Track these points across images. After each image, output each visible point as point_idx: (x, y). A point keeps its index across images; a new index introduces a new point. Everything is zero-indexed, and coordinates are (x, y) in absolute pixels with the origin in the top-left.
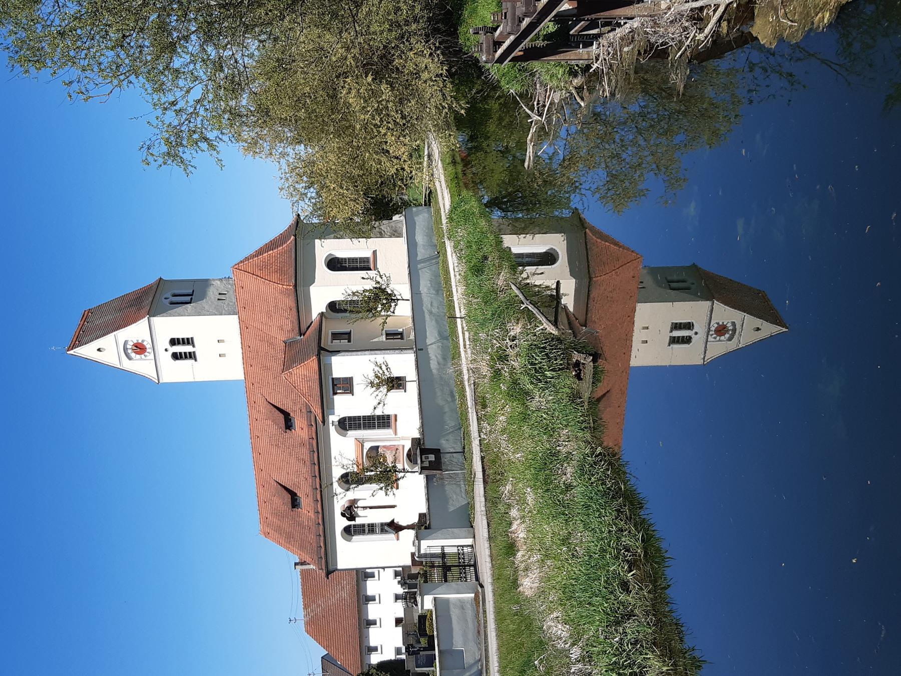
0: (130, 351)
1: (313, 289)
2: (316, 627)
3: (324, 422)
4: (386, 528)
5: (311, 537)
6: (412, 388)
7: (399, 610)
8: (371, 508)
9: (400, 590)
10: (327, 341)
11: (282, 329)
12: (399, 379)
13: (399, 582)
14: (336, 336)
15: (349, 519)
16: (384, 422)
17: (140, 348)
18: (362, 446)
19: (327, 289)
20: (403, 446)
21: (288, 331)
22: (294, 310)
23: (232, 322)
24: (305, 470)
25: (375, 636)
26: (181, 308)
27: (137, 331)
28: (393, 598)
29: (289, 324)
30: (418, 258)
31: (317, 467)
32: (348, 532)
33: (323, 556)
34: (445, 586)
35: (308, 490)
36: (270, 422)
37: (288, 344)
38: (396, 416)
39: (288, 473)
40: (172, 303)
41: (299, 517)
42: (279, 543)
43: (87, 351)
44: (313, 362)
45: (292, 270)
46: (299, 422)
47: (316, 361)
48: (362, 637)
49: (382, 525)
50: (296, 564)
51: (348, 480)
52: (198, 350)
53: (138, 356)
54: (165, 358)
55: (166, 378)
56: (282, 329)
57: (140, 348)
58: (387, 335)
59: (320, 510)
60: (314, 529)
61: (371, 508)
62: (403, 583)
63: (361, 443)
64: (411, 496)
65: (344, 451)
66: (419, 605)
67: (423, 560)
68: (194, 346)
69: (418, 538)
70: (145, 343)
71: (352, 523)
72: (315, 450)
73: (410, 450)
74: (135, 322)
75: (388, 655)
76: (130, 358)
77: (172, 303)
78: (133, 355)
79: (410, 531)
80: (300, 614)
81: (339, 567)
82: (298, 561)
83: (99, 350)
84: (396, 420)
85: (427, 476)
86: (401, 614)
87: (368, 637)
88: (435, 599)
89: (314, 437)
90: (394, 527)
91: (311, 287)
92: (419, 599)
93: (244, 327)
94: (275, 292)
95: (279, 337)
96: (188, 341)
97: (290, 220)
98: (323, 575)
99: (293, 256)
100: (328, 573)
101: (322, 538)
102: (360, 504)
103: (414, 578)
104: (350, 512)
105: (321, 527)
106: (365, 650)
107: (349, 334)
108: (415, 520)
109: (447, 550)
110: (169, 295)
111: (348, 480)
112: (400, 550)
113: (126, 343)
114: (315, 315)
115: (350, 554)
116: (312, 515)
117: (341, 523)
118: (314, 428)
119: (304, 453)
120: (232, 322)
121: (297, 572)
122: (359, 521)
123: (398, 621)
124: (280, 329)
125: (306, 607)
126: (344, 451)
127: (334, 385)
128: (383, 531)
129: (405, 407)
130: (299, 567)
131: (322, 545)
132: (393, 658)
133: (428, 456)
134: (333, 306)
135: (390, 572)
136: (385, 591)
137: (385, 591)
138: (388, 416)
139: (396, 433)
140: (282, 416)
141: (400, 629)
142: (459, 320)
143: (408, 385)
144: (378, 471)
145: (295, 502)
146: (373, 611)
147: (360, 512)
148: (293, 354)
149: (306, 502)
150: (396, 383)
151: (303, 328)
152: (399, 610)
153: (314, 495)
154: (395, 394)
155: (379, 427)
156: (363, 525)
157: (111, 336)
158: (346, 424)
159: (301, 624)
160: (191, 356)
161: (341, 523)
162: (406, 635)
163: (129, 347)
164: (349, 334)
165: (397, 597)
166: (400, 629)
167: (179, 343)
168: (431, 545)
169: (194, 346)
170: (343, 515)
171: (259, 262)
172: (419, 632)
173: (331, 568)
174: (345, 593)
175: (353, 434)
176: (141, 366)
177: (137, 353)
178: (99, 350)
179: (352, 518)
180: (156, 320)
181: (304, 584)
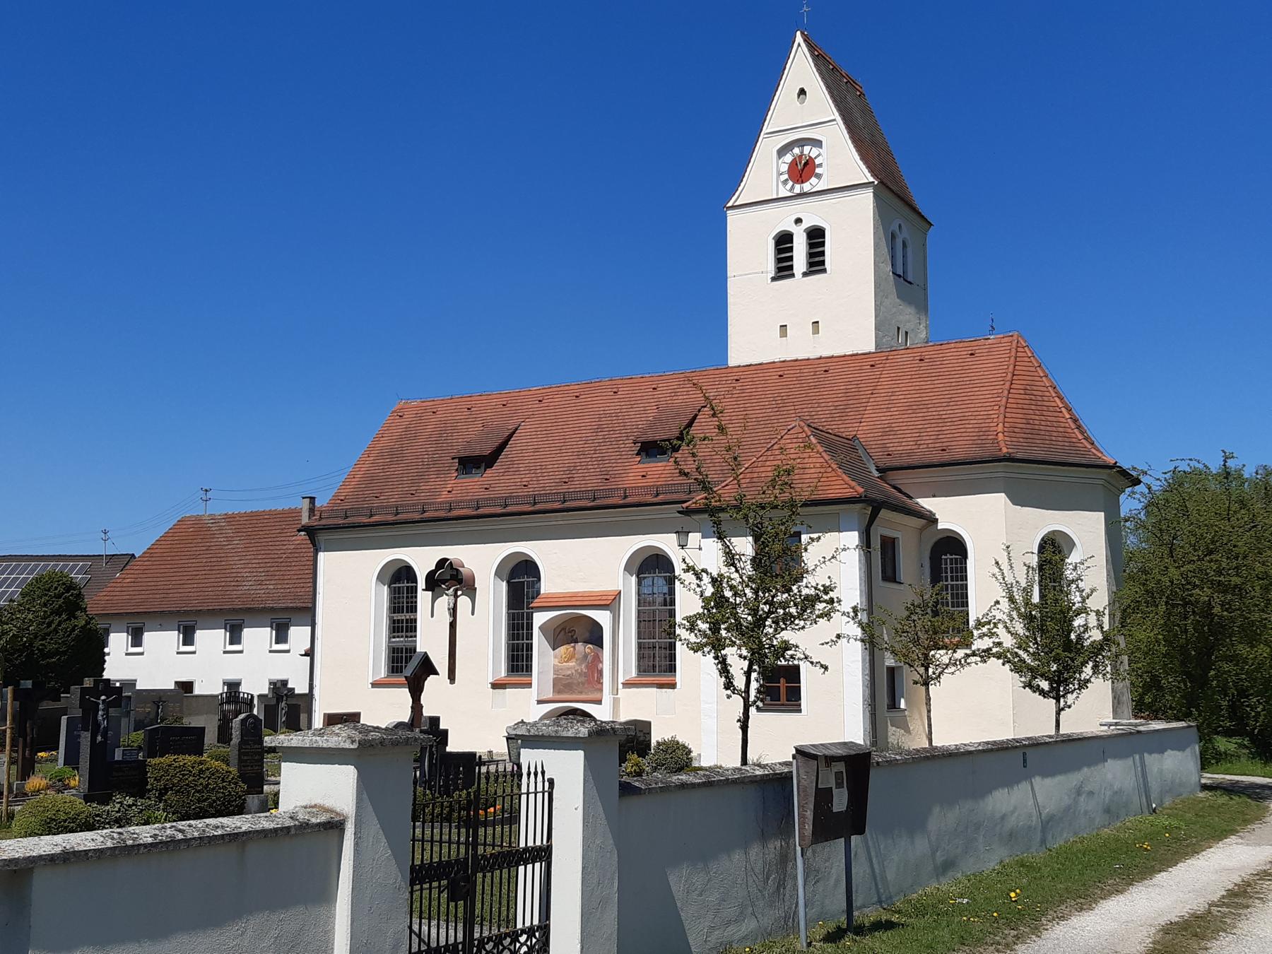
0: (797, 151)
1: (998, 501)
2: (190, 538)
5: (392, 497)
8: (453, 626)
10: (890, 523)
11: (885, 433)
14: (889, 546)
15: (430, 577)
17: (802, 170)
19: (993, 532)
20: (599, 702)
21: (884, 446)
22: (946, 457)
23: (864, 341)
24: (547, 483)
25: (161, 642)
26: (885, 250)
27: (841, 159)
28: (232, 677)
29: (903, 446)
30: (1146, 755)
31: (557, 505)
32: (400, 578)
33: (350, 520)
34: (394, 877)
35: (501, 490)
36: (652, 413)
38: (673, 686)
39: (536, 450)
40: (893, 236)
41: (438, 473)
42: (378, 439)
43: (801, 67)
44: (841, 486)
45: (1040, 455)
47: (848, 493)
48: (161, 619)
50: (312, 499)
51: (521, 579)
52: (799, 282)
53: (785, 168)
55: (735, 222)
56: (885, 433)
57: (802, 170)
58: (891, 671)
59: (455, 513)
60: (411, 500)
61: (453, 626)
63: (611, 603)
68: (805, 274)
70: (813, 180)
71: (421, 584)
72: (598, 502)
74: (864, 158)
76: (782, 152)
77: (893, 236)
78: (788, 158)
80: (220, 507)
81: (321, 555)
82: (318, 504)
83: (802, 92)
84: (661, 686)
85: (787, 778)
87: (162, 628)
88: (334, 826)
89: (629, 500)
91: (1002, 496)
94: (983, 417)
95: (864, 427)
96: (816, 263)
99: (1071, 460)
101: (391, 518)
102: (464, 601)
104: (449, 578)
106: (137, 622)
111: (521, 579)
113: (817, 143)
114: (927, 503)
115: (349, 582)
116: (444, 497)
117: (422, 559)
118: (650, 499)
119: (587, 481)
120: (864, 341)
122: (424, 597)
123: (186, 686)
124: (884, 428)
125: (230, 518)
126: (585, 566)
130: (305, 504)
134: (950, 551)
136: (248, 663)
137: (248, 663)
138: (672, 669)
139: (627, 685)
145: (470, 463)
146: (211, 639)
147: (444, 602)
149: (474, 485)
151: (901, 479)
153: (491, 501)
155: (640, 647)
156: (413, 609)
160: (784, 269)
161: (422, 559)
162: (157, 697)
163: (807, 149)
167: (811, 246)
169: (805, 274)
170: (442, 563)
171: (1030, 393)
173: (322, 538)
174: (251, 588)
175: (628, 587)
176: (764, 171)
177: (793, 165)
178: (802, 92)
179: (433, 583)
180: (867, 197)
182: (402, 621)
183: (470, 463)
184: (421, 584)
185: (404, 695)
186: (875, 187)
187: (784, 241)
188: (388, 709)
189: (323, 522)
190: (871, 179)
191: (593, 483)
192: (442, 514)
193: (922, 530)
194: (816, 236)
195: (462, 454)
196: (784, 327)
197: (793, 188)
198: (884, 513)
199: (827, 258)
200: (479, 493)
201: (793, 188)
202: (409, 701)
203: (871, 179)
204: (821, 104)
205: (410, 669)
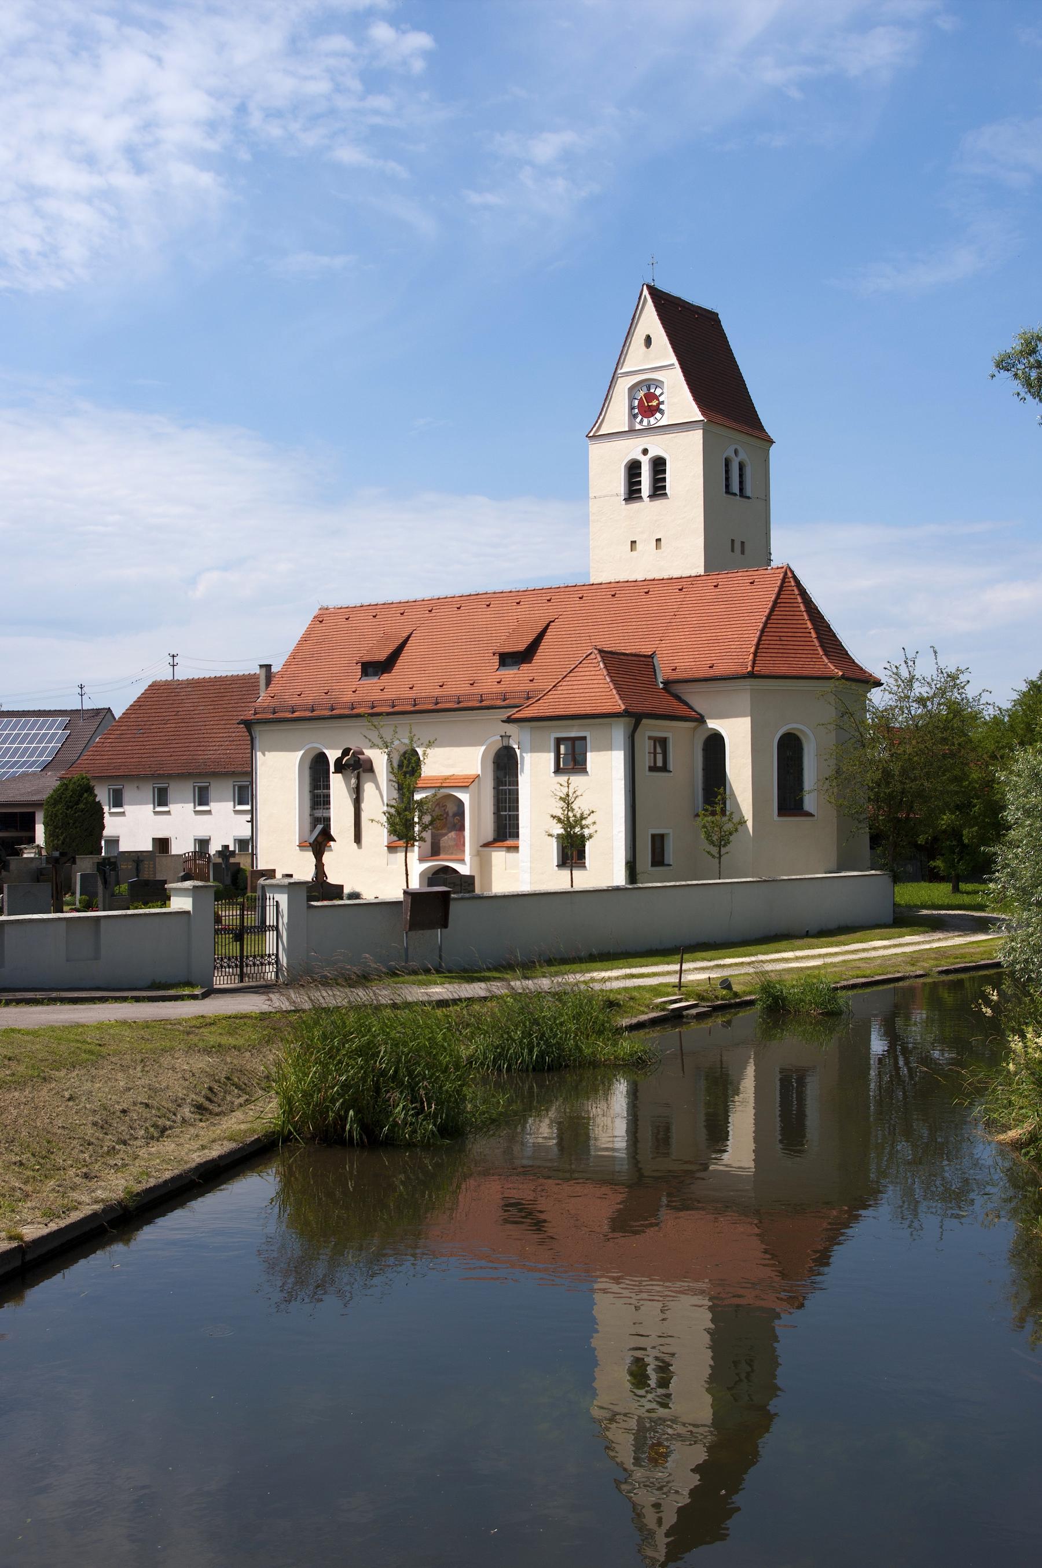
2: (163, 699)
3: (509, 720)
4: (320, 827)
6: (558, 880)
7: (182, 846)
9: (214, 848)
10: (651, 729)
12: (581, 855)
13: (227, 847)
15: (338, 761)
16: (505, 830)
18: (464, 788)
22: (711, 673)
28: (202, 834)
37: (646, 662)
46: (515, 677)
49: (328, 820)
51: (407, 767)
52: (646, 506)
54: (632, 449)
62: (225, 852)
63: (467, 783)
64: (376, 871)
65: (455, 761)
66: (179, 885)
67: (259, 893)
69: (293, 887)
70: (658, 415)
71: (332, 769)
73: (457, 872)
75: (112, 825)
76: (632, 389)
77: (727, 463)
79: (250, 834)
82: (274, 670)
86: (176, 849)
90: (320, 841)
92: (188, 884)
93: (682, 584)
96: (659, 490)
97: (876, 670)
98: (249, 715)
100: (248, 724)
101: (308, 714)
103: (231, 877)
105: (328, 713)
107: (664, 769)
108: (332, 879)
109: (270, 936)
110: (743, 456)
111: (407, 767)
112: (283, 855)
119: (458, 687)
121: (250, 667)
126: (455, 761)
127: (573, 740)
128: (315, 821)
129: (524, 869)
130: (263, 674)
131: (296, 714)
132: (106, 833)
133: (435, 904)
135: (245, 832)
136: (221, 824)
140: (521, 647)
141: (148, 846)
142: (677, 967)
143: (566, 873)
144: (421, 818)
145: (372, 668)
148: (628, 668)
149: (373, 688)
150: (572, 851)
152: (182, 846)
154: (552, 850)
157: (673, 359)
158: (505, 766)
159: (164, 674)
160: (633, 493)
162: (137, 858)
164: (664, 769)
165: (203, 843)
166: (148, 846)
168: (279, 904)
172: (143, 878)
173: (257, 730)
180: (697, 436)
181: (235, 680)
182: (318, 798)
183: (372, 668)
184: (332, 769)
185: (310, 857)
186: (705, 424)
187: (633, 469)
188: (305, 872)
189: (258, 716)
190: (702, 418)
191: (463, 689)
192: (347, 712)
193: (695, 729)
194: (659, 465)
195: (366, 659)
196: (633, 543)
197: (641, 422)
198: (644, 721)
199: (668, 484)
200: (376, 696)
201: (641, 422)
202: (313, 860)
203: (702, 418)
204: (664, 352)
205: (320, 841)
